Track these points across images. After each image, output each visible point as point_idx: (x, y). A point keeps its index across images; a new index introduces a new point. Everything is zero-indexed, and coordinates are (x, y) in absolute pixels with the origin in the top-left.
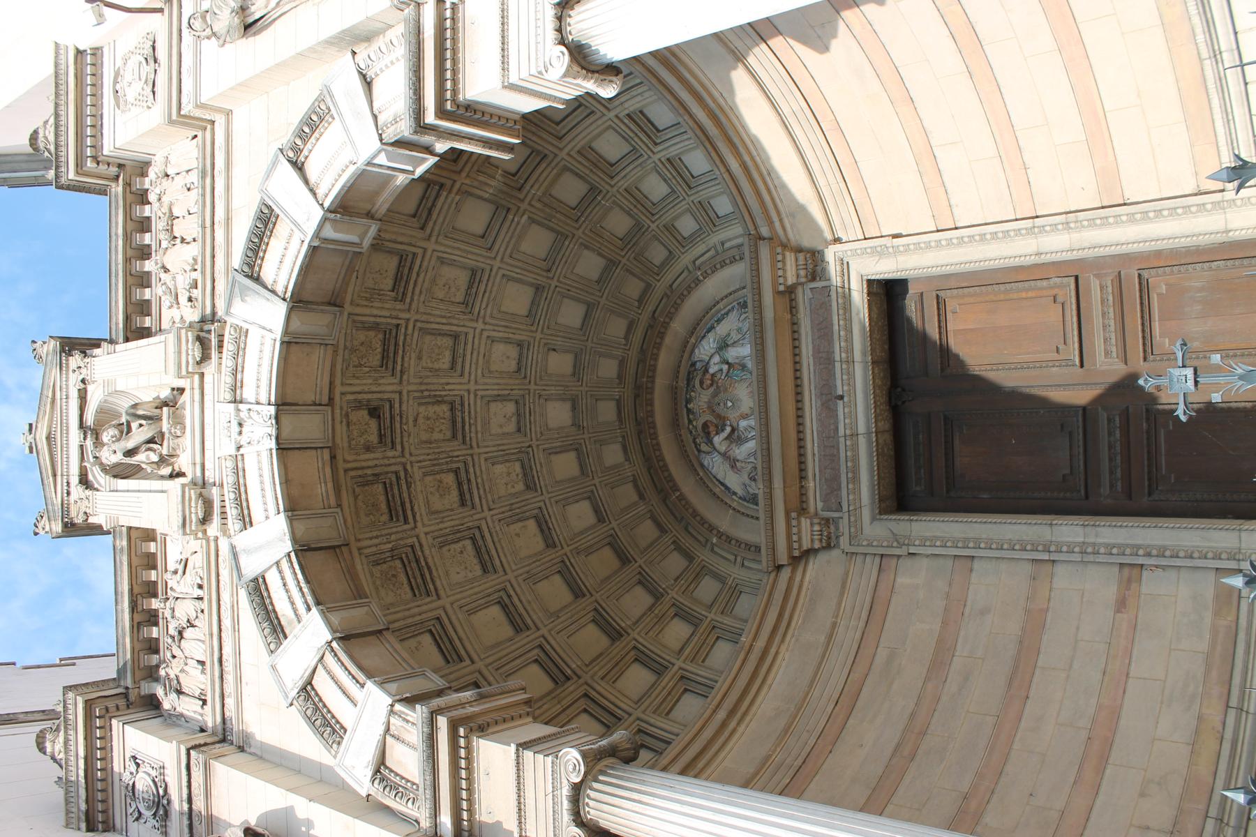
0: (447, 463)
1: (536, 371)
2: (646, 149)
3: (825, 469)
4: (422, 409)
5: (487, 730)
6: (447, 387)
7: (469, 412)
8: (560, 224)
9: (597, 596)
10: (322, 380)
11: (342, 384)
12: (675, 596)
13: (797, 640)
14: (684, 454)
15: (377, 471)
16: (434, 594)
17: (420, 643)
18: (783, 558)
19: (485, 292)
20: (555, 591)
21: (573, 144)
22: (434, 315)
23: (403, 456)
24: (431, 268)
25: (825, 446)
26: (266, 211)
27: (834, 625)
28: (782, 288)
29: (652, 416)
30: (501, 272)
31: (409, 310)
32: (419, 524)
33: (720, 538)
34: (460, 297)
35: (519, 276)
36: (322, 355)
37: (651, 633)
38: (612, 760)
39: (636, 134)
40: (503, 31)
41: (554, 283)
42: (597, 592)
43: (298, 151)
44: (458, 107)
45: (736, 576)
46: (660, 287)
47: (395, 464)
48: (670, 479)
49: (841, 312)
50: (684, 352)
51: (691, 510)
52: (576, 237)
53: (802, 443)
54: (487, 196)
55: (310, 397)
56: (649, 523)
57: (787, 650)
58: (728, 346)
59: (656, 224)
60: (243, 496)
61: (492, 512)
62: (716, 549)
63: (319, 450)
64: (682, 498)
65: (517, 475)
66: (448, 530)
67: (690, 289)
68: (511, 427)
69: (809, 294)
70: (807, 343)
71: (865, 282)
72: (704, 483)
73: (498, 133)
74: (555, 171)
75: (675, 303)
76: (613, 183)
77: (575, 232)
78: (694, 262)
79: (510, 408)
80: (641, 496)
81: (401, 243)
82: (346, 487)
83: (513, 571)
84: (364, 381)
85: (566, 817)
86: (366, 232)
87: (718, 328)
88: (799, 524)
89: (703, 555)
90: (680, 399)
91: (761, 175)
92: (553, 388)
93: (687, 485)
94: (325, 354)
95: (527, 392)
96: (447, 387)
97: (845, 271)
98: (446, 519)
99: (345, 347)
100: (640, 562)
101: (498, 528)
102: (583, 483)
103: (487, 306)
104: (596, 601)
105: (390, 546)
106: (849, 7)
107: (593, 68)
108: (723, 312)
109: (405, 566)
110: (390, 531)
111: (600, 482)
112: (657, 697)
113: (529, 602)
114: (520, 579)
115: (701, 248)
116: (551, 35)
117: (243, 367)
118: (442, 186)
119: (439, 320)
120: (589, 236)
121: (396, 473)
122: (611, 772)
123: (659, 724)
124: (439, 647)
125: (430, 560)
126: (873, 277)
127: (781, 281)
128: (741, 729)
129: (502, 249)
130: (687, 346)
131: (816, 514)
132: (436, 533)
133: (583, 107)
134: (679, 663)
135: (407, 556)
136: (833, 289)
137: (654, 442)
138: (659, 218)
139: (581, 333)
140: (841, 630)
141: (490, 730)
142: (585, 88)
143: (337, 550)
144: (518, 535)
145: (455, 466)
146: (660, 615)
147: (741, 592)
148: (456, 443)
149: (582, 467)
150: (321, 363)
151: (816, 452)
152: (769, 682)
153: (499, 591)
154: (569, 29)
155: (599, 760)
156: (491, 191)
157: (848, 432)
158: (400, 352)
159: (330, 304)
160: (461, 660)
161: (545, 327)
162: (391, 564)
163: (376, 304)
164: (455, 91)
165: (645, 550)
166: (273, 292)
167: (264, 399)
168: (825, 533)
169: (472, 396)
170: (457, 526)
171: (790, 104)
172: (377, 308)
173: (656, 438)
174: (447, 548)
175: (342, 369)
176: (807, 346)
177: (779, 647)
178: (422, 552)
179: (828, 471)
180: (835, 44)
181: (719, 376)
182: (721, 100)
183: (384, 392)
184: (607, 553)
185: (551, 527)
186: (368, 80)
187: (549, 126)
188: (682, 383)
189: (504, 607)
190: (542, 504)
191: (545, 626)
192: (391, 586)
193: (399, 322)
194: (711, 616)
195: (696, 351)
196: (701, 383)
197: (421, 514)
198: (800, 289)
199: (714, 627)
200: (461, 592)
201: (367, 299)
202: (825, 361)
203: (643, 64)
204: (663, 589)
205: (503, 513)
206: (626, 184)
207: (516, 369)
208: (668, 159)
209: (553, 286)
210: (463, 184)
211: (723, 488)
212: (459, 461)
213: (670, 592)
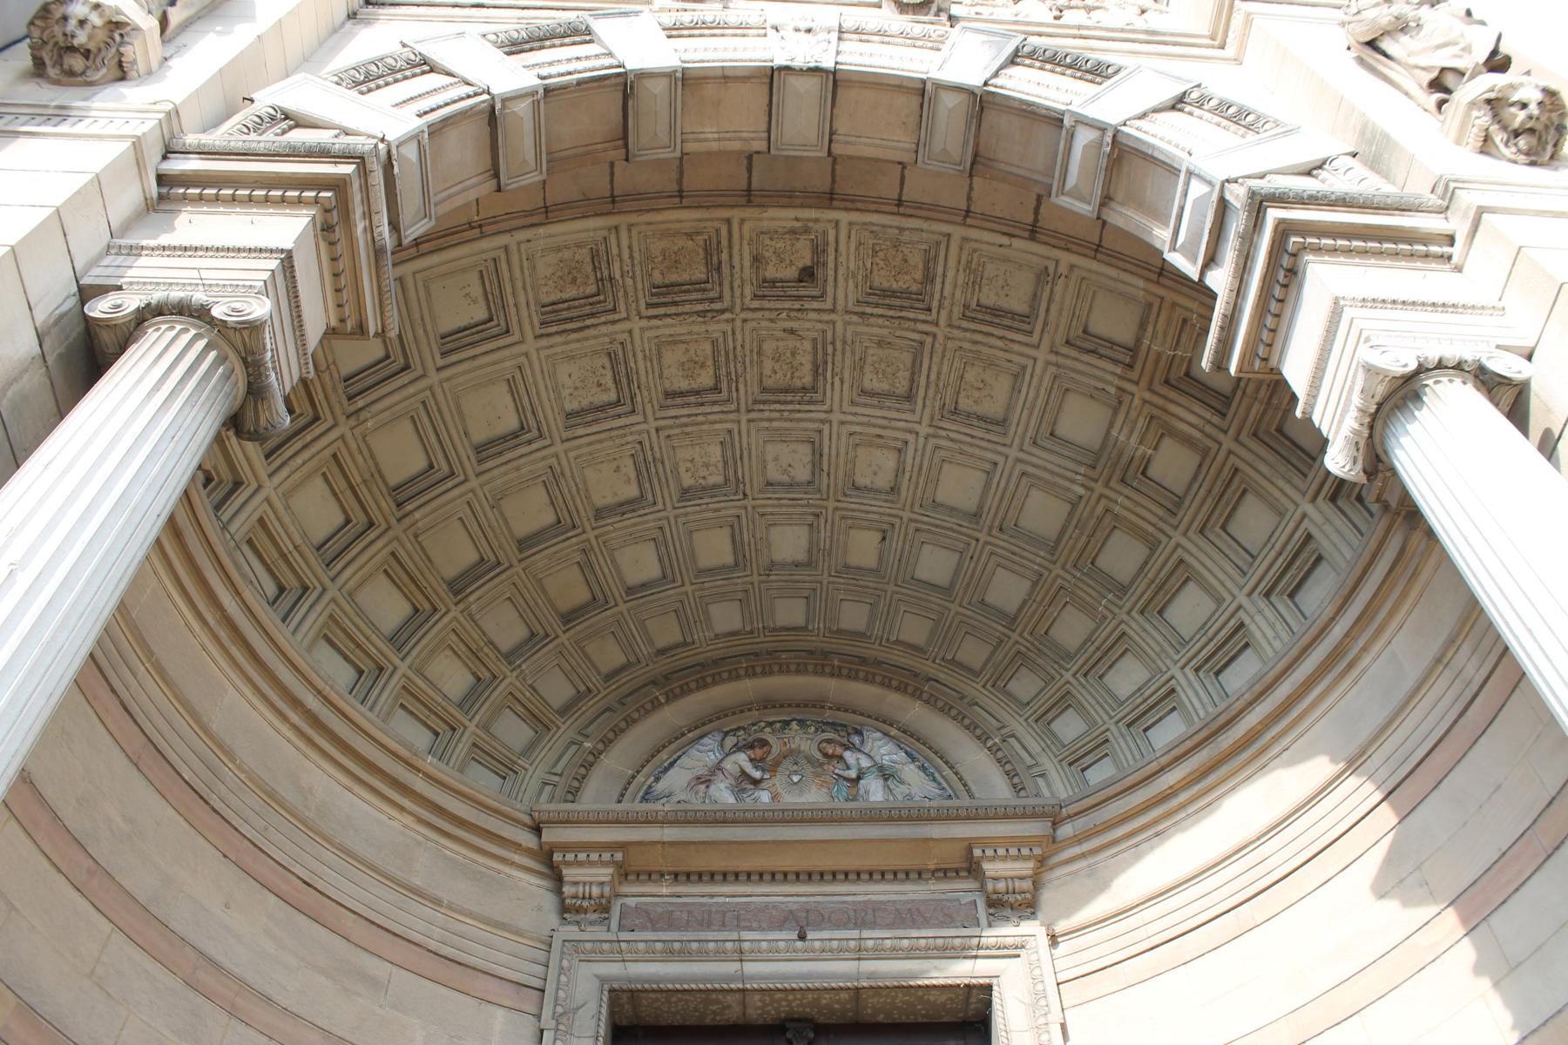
0: (729, 374)
1: (853, 510)
2: (1189, 655)
3: (689, 912)
4: (808, 345)
5: (324, 240)
6: (837, 379)
7: (799, 411)
8: (1071, 542)
9: (518, 569)
10: (866, 144)
11: (851, 224)
12: (507, 681)
13: (419, 843)
14: (722, 713)
15: (725, 269)
16: (544, 331)
17: (475, 302)
18: (550, 835)
19: (972, 437)
20: (532, 511)
21: (1194, 550)
22: (942, 364)
23: (743, 310)
24: (1009, 356)
25: (724, 913)
26: (1110, 71)
27: (437, 902)
28: (977, 852)
29: (781, 672)
30: (1001, 460)
31: (950, 326)
32: (644, 323)
33: (591, 753)
34: (965, 403)
35: (994, 486)
36: (901, 145)
37: (454, 638)
38: (242, 387)
39: (1211, 640)
40: (1423, 304)
41: (983, 537)
42: (524, 570)
43: (1200, 104)
44: (1294, 255)
45: (530, 772)
46: (973, 689)
47: (732, 296)
48: (686, 691)
49: (940, 942)
50: (877, 719)
51: (636, 715)
52: (1051, 566)
53: (731, 878)
54: (1114, 433)
55: (842, 127)
56: (620, 659)
57: (405, 826)
58: (886, 780)
59: (1072, 680)
60: (707, 32)
61: (653, 432)
62: (574, 748)
63: (766, 135)
64: (656, 705)
65: (704, 478)
66: (632, 365)
67: (971, 728)
68: (773, 474)
69: (970, 897)
70: (889, 893)
71: (987, 981)
72: (677, 739)
73: (1248, 333)
74: (1151, 529)
75: (952, 707)
76: (1134, 613)
77: (1058, 564)
78: (1013, 736)
79: (803, 474)
80: (662, 652)
81: (1048, 310)
82: (707, 220)
83: (566, 452)
84: (852, 258)
85: (157, 296)
86: (1081, 199)
87: (912, 766)
88: (604, 864)
89: (566, 730)
90: (805, 710)
91: (1156, 822)
92: (829, 534)
93: (673, 715)
94: (903, 150)
95: (825, 496)
96: (837, 379)
97: (1005, 952)
98: (649, 364)
99: (901, 230)
100: (564, 638)
101: (630, 438)
102: (687, 570)
103: (952, 440)
104: (511, 566)
105: (618, 276)
106: (1464, 920)
107: (1378, 425)
108: (937, 775)
109: (587, 297)
110: (639, 279)
111: (687, 593)
112: (355, 625)
113: (518, 469)
114: (553, 461)
115: (1035, 747)
116: (1433, 354)
117: (889, 43)
118: (1131, 366)
119: (935, 369)
120: (1052, 585)
121: (720, 298)
122: (220, 370)
123: (312, 617)
124: (465, 329)
125: (592, 332)
126: (995, 993)
127: (989, 852)
128: (285, 729)
129: (1034, 460)
130: (886, 723)
131: (618, 895)
132: (629, 347)
133: (1250, 560)
134: (403, 667)
135: (600, 302)
136: (976, 931)
137: (742, 672)
138: (1081, 684)
139: (908, 578)
140: (427, 911)
141: (323, 245)
142: (1335, 438)
143: (621, 142)
144: (617, 469)
145: (724, 386)
146: (480, 655)
147: (504, 778)
148: (756, 389)
149: (711, 571)
150: (890, 144)
151: (715, 900)
152: (357, 789)
153: (539, 430)
154: (1445, 379)
155: (244, 361)
156: (1122, 438)
157: (746, 945)
158: (891, 313)
159: (976, 155)
160: (444, 354)
161: (919, 525)
162: (592, 280)
163: (961, 276)
164: (1318, 250)
165: (582, 649)
166: (996, 75)
167: (840, 59)
168: (585, 904)
169: (823, 416)
170: (638, 379)
171: (1278, 854)
172: (956, 279)
173: (747, 675)
174: (608, 365)
175: (872, 224)
176: (884, 893)
177: (410, 813)
178: (604, 323)
179: (685, 916)
180: (1392, 906)
181: (839, 765)
182: (1276, 749)
183: (836, 286)
184: (583, 595)
185: (626, 516)
186: (1315, 172)
187: (1221, 515)
188: (828, 715)
189: (515, 435)
190: (660, 506)
191: (481, 486)
192: (559, 274)
193: (934, 311)
194: (472, 727)
195: (879, 734)
196: (829, 741)
197: (658, 327)
198: (973, 885)
199: (454, 729)
200: (542, 372)
201: (969, 262)
202: (862, 917)
203: (1333, 619)
204: (520, 666)
205: (652, 449)
206: (1132, 633)
207: (857, 484)
208: (1173, 691)
209: (978, 535)
210: (1133, 395)
211: (666, 764)
212: (730, 391)
213: (515, 674)
